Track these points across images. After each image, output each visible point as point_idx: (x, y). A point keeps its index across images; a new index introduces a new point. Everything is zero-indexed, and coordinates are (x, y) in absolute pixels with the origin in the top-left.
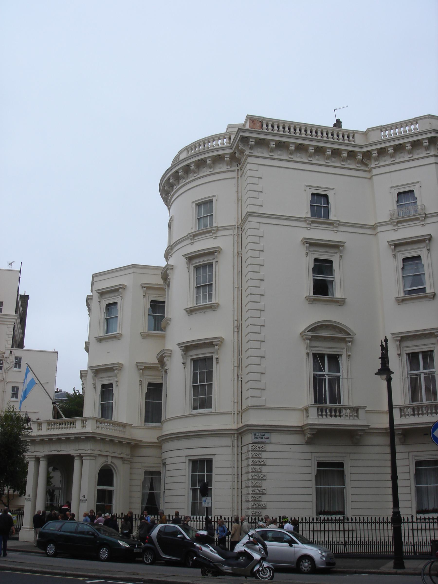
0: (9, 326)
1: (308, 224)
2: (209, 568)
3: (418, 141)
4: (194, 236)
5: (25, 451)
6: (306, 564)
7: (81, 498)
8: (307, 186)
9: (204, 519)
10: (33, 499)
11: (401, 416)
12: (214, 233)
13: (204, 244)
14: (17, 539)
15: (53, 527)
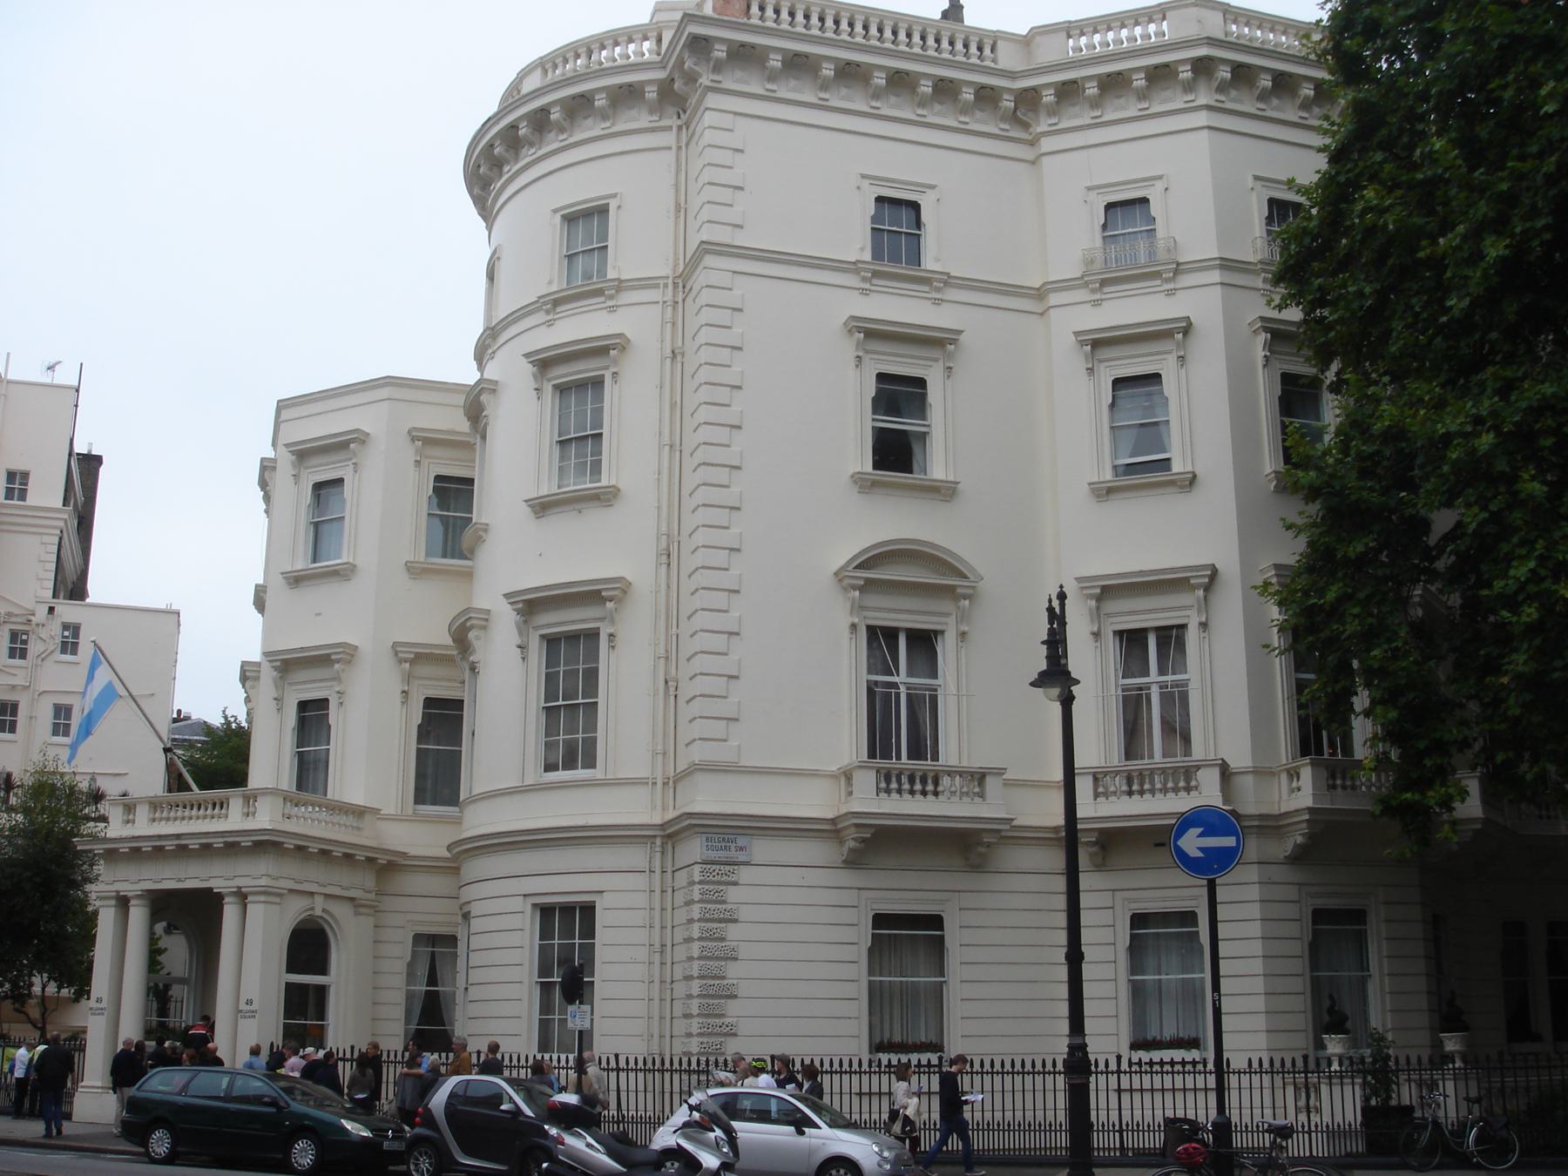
0: (46, 539)
1: (864, 279)
3: (1166, 65)
4: (557, 303)
7: (243, 1006)
8: (864, 176)
9: (571, 1063)
11: (1096, 795)
12: (611, 297)
15: (162, 1083)
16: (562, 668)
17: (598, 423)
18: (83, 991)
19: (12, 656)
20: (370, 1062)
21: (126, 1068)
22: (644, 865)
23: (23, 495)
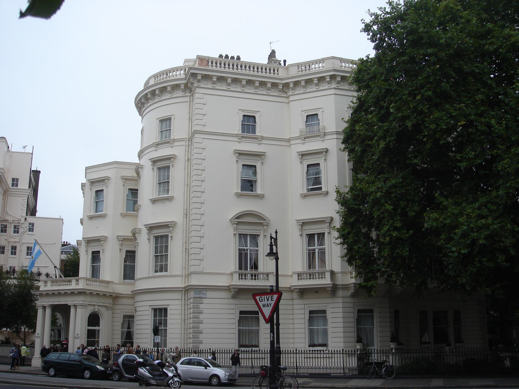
0: (24, 198)
1: (239, 139)
4: (158, 145)
5: (36, 300)
6: (215, 380)
7: (76, 336)
8: (239, 110)
10: (42, 334)
11: (298, 279)
12: (172, 144)
13: (164, 152)
14: (30, 365)
15: (53, 356)
18: (34, 332)
19: (14, 233)
20: (107, 350)
21: (44, 352)
22: (179, 297)
23: (17, 186)
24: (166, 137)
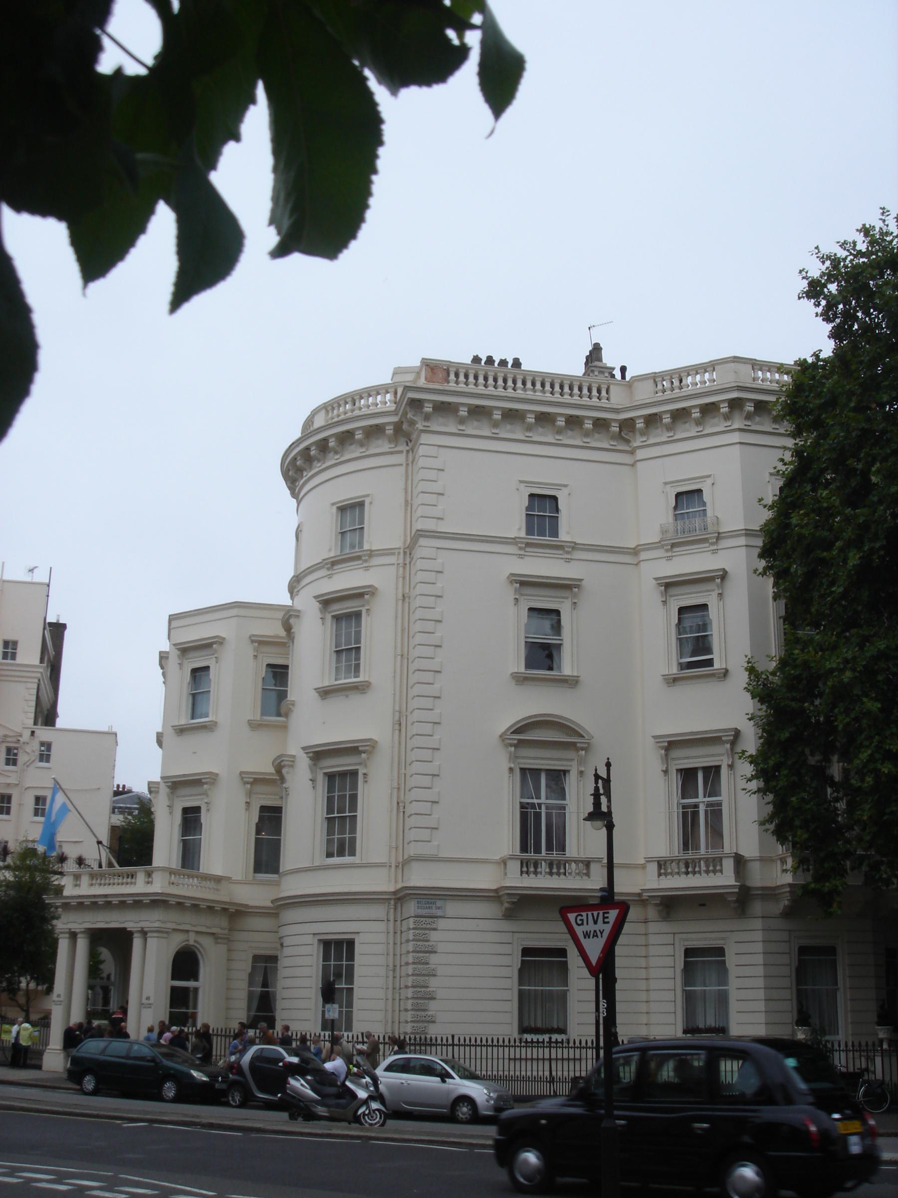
0: (29, 685)
1: (520, 549)
2: (297, 1108)
3: (713, 404)
4: (334, 564)
7: (144, 1001)
8: (521, 482)
9: (327, 1038)
10: (68, 997)
11: (660, 875)
12: (366, 561)
14: (39, 1067)
15: (92, 1047)
16: (336, 793)
17: (358, 641)
19: (7, 764)
21: (71, 1038)
23: (14, 656)
24: (353, 546)
